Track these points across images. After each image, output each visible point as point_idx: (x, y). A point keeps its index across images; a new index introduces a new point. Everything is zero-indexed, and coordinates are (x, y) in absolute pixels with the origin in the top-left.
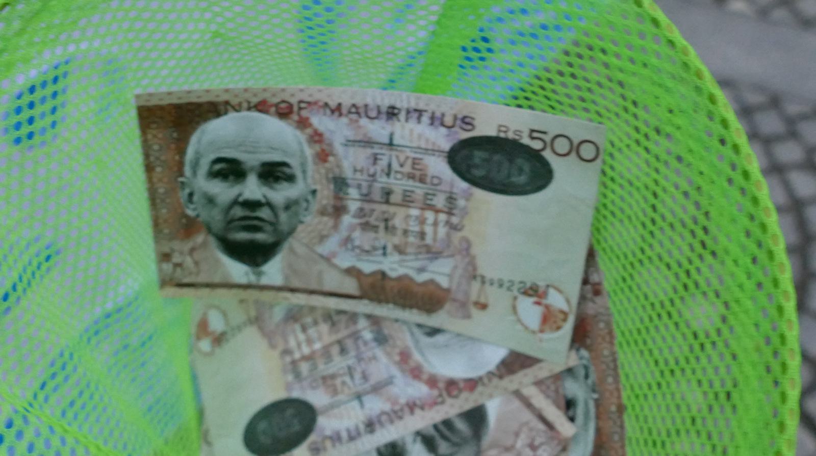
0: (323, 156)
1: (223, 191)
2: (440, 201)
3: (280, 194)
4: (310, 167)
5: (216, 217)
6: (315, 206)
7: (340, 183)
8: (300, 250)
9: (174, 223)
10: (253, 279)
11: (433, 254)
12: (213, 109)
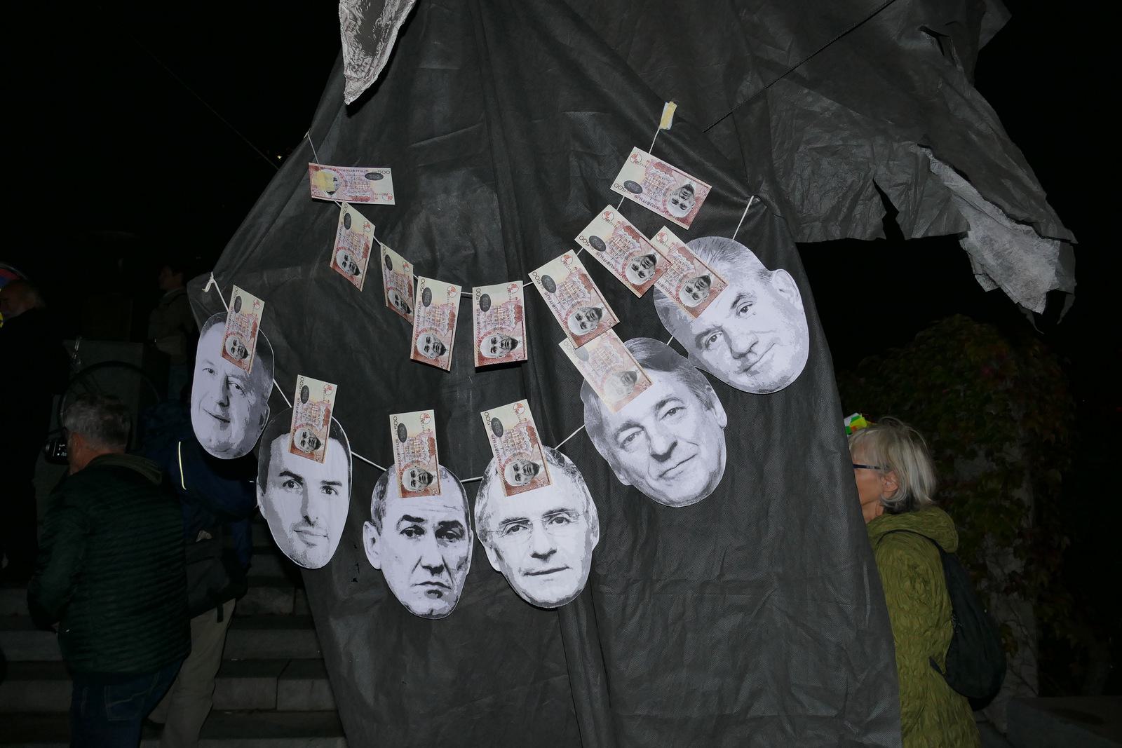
0: (409, 466)
1: (418, 484)
2: (510, 435)
3: (417, 473)
4: (513, 462)
5: (423, 485)
6: (521, 458)
7: (514, 455)
8: (532, 458)
9: (534, 485)
10: (436, 478)
11: (422, 442)
12: (506, 483)
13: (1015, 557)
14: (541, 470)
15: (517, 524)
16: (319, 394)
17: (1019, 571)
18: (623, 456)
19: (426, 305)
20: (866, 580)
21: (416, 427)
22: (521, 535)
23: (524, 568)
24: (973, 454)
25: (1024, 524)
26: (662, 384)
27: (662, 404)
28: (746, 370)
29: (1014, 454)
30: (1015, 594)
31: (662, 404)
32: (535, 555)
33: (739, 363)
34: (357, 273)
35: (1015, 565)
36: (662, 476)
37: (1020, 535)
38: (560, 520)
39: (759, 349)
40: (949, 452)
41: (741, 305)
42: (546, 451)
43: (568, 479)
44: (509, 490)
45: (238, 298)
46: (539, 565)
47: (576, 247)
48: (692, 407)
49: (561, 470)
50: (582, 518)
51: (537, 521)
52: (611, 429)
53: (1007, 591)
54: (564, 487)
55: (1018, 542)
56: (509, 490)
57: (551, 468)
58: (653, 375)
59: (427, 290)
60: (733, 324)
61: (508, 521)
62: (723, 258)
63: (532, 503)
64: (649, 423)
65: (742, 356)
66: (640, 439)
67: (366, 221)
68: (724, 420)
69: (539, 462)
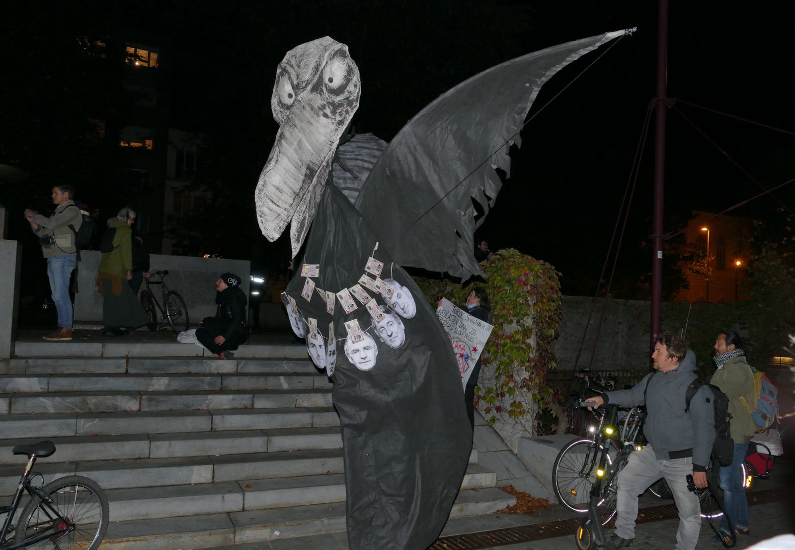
9: (360, 341)
13: (526, 371)
14: (361, 337)
15: (357, 351)
16: (313, 322)
17: (528, 378)
18: (382, 335)
19: (342, 299)
20: (641, 156)
21: (353, 325)
22: (357, 354)
23: (359, 361)
24: (511, 322)
25: (531, 356)
26: (388, 318)
27: (388, 323)
28: (405, 312)
29: (529, 322)
30: (525, 389)
31: (388, 323)
32: (362, 358)
33: (403, 311)
34: (309, 297)
35: (526, 375)
36: (390, 340)
37: (529, 361)
38: (367, 349)
39: (406, 307)
40: (501, 320)
41: (399, 296)
42: (362, 332)
43: (369, 338)
44: (353, 342)
45: (328, 295)
46: (363, 361)
47: (359, 283)
48: (396, 324)
49: (366, 337)
50: (373, 348)
51: (361, 350)
52: (378, 328)
53: (522, 387)
54: (368, 341)
55: (527, 364)
56: (353, 342)
57: (364, 336)
58: (386, 315)
59: (352, 290)
60: (398, 301)
61: (353, 351)
62: (392, 284)
63: (360, 345)
64: (386, 327)
65: (403, 309)
66: (384, 331)
67: (313, 282)
68: (404, 328)
69: (361, 335)
